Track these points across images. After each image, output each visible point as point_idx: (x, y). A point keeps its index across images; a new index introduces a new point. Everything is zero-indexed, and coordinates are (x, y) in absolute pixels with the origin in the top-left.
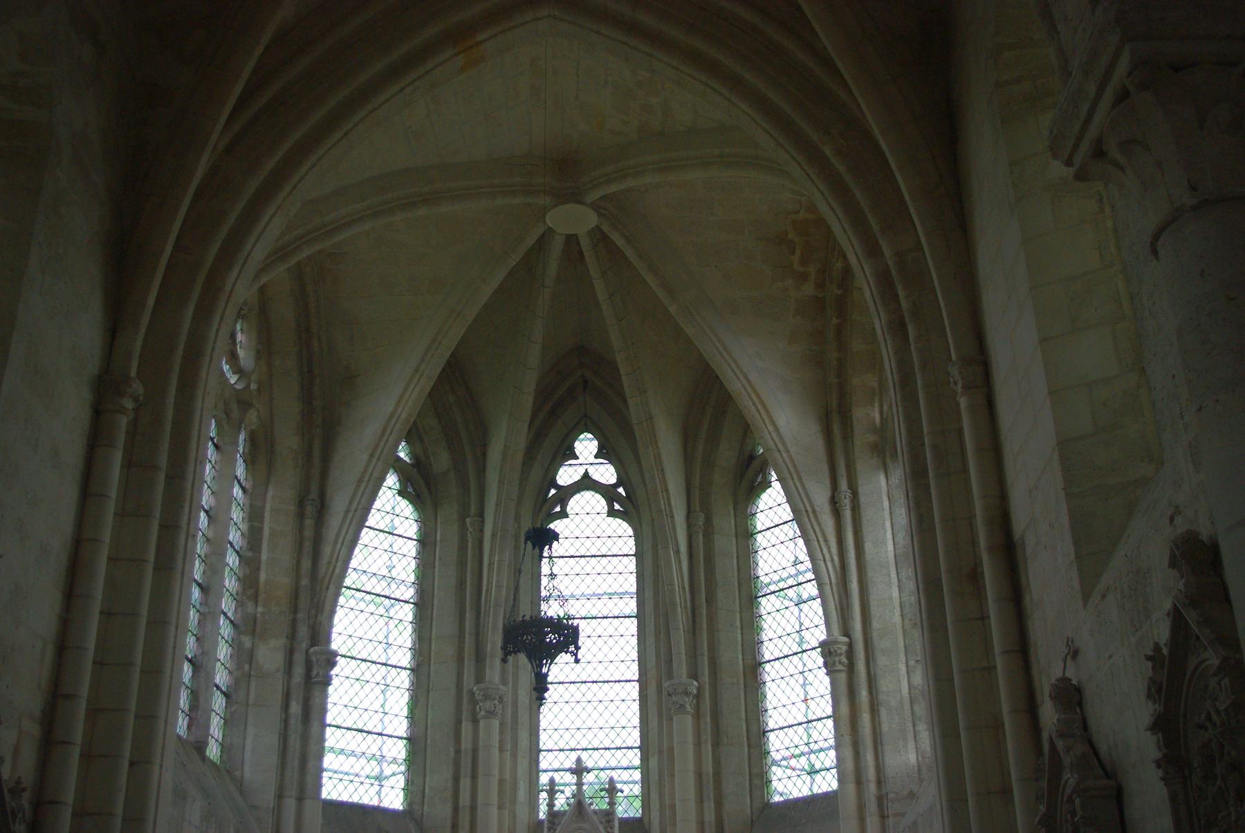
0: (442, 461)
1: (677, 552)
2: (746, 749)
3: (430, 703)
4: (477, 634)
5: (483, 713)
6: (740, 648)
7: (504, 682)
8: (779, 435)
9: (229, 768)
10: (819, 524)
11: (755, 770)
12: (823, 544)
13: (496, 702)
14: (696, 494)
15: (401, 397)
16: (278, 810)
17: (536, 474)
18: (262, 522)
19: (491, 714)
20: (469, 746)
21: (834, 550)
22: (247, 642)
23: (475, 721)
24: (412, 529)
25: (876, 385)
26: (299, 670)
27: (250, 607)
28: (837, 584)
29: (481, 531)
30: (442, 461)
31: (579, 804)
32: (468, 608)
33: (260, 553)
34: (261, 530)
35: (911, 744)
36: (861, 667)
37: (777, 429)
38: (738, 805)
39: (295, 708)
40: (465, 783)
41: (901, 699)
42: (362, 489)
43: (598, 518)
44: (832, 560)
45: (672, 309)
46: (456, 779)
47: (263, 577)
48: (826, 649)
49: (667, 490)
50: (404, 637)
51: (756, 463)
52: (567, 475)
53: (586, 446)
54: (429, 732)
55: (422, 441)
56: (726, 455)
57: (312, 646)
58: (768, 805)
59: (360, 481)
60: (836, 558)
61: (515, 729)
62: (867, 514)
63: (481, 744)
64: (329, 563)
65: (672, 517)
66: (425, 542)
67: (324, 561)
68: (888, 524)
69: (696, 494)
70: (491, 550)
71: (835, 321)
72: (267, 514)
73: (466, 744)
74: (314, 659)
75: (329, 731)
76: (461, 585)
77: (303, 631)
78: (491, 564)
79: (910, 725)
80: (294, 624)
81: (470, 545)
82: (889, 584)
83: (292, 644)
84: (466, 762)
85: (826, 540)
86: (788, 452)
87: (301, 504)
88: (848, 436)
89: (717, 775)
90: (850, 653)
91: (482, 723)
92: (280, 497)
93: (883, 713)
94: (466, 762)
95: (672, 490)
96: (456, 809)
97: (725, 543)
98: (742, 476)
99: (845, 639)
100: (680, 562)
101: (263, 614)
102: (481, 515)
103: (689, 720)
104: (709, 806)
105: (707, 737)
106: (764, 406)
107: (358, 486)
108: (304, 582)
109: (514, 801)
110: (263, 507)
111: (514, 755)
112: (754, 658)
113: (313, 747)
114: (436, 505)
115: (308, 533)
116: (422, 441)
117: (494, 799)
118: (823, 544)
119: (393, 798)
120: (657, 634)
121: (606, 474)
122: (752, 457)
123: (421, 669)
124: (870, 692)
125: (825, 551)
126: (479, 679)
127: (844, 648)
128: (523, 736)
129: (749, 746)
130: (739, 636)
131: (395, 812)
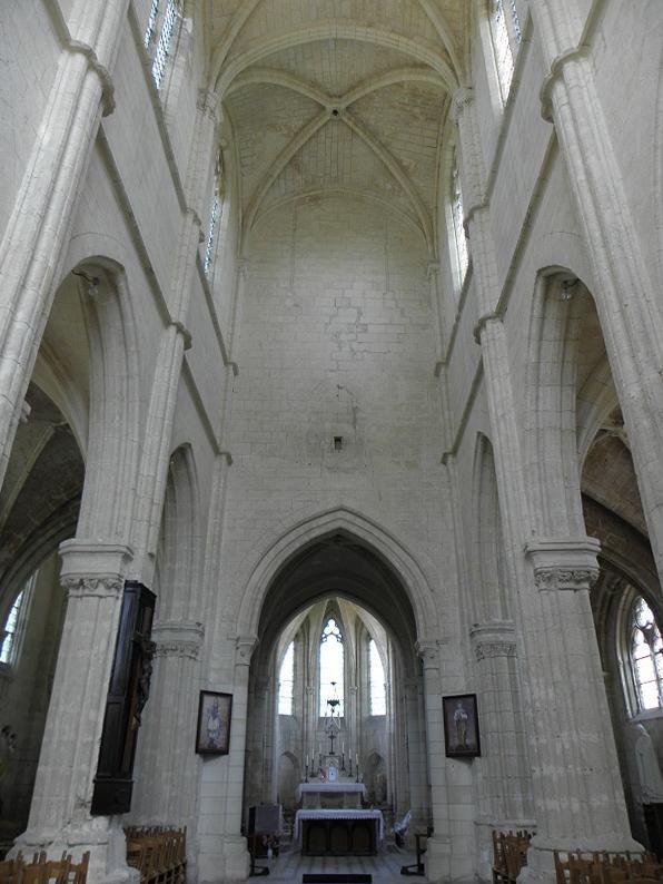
38: (365, 715)
58: (371, 716)
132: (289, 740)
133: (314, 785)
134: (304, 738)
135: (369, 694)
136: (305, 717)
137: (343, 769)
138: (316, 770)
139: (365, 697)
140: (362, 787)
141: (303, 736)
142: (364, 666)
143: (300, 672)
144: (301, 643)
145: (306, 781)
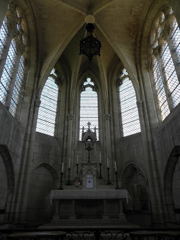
1: (106, 92)
7: (73, 114)
8: (128, 65)
9: (16, 118)
10: (136, 82)
11: (121, 131)
14: (109, 84)
15: (55, 56)
16: (27, 129)
17: (80, 82)
18: (27, 76)
19: (71, 119)
20: (67, 125)
22: (22, 96)
23: (68, 121)
24: (57, 89)
25: (146, 57)
26: (33, 103)
27: (23, 90)
29: (70, 89)
30: (63, 78)
31: (89, 130)
33: (26, 81)
34: (27, 77)
35: (157, 119)
36: (145, 105)
37: (128, 64)
39: (32, 110)
40: (66, 131)
41: (154, 110)
43: (91, 91)
44: (138, 88)
45: (108, 40)
46: (64, 131)
47: (26, 85)
50: (56, 107)
52: (85, 84)
53: (89, 80)
55: (59, 74)
56: (115, 78)
58: (123, 137)
61: (75, 123)
62: (145, 79)
63: (69, 124)
66: (59, 91)
68: (150, 81)
69: (109, 84)
71: (139, 45)
72: (28, 75)
73: (66, 124)
74: (36, 101)
76: (66, 98)
77: (34, 96)
78: (72, 94)
79: (156, 115)
80: (32, 96)
82: (151, 91)
84: (66, 128)
85: (137, 84)
87: (35, 75)
89: (114, 131)
90: (143, 103)
92: (32, 71)
93: (151, 113)
94: (66, 128)
96: (64, 136)
97: (114, 93)
98: (117, 82)
101: (26, 92)
103: (109, 121)
104: (113, 136)
105: (112, 124)
106: (125, 60)
107: (47, 71)
109: (75, 136)
110: (27, 74)
111: (75, 128)
113: (35, 118)
114: (62, 86)
116: (59, 74)
117: (71, 134)
119: (52, 134)
120: (102, 108)
121: (92, 84)
122: (119, 79)
123: (59, 102)
124: (147, 110)
126: (69, 113)
127: (142, 103)
128: (77, 125)
134: (64, 154)
136: (65, 138)
137: (100, 178)
140: (124, 194)
141: (62, 153)
142: (115, 101)
143: (63, 104)
144: (64, 86)
145: (61, 188)
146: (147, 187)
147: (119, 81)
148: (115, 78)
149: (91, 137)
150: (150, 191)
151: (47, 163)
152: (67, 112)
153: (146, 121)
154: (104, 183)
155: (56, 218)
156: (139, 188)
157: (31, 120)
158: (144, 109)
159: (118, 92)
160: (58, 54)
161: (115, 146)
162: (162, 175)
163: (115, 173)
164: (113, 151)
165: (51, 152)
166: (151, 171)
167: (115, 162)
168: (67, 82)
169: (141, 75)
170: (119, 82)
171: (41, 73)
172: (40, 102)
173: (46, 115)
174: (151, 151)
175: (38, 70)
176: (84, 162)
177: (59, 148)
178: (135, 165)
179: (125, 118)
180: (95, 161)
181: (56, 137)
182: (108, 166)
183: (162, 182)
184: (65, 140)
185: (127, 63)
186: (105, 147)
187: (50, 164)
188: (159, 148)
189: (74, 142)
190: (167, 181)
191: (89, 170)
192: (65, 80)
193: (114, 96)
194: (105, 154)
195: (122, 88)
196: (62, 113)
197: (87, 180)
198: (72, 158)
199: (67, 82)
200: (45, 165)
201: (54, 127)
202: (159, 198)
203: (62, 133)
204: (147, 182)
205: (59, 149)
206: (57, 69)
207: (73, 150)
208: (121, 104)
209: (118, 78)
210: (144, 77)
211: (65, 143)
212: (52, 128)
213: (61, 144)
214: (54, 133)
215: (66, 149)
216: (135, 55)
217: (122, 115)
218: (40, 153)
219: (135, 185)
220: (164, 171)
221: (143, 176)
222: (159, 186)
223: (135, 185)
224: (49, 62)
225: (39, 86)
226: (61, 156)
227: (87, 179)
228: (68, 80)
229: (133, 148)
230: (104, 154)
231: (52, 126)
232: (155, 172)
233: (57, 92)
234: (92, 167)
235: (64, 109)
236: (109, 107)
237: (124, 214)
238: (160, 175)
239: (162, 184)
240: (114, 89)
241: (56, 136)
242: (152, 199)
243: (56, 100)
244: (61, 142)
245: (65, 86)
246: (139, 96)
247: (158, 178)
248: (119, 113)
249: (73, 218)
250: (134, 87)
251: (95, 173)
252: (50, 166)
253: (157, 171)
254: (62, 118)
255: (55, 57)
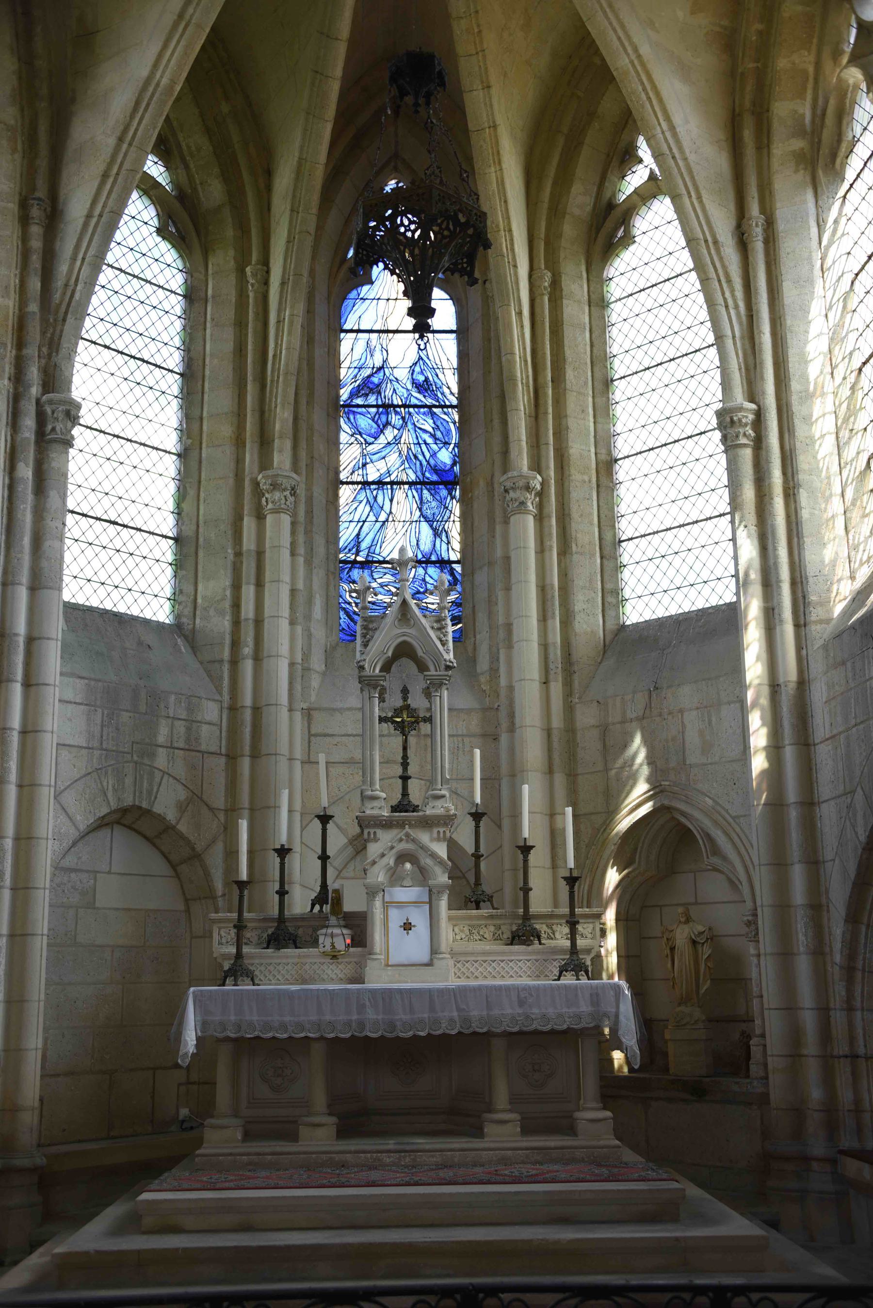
0: (213, 192)
1: (520, 314)
2: (599, 561)
3: (202, 495)
4: (262, 412)
5: (270, 506)
6: (592, 440)
8: (675, 135)
10: (721, 259)
11: (609, 586)
12: (725, 285)
13: (287, 493)
15: (160, 56)
21: (739, 294)
23: (260, 517)
24: (177, 281)
26: (29, 423)
28: (742, 338)
30: (213, 192)
32: (250, 378)
38: (589, 623)
40: (248, 592)
42: (108, 186)
44: (736, 307)
46: (236, 587)
48: (726, 421)
49: (510, 230)
50: (171, 414)
51: (616, 214)
54: (201, 530)
55: (187, 167)
56: (580, 200)
57: (43, 394)
58: (623, 627)
59: (105, 176)
60: (742, 305)
64: (66, 285)
65: (515, 266)
67: (59, 283)
70: (280, 303)
73: (249, 543)
74: (49, 410)
75: (82, 344)
76: (240, 350)
77: (34, 373)
81: (251, 301)
83: (16, 389)
85: (729, 281)
86: (685, 159)
87: (24, 205)
88: (764, 143)
91: (269, 519)
95: (516, 233)
96: (236, 623)
97: (575, 311)
98: (598, 230)
99: (753, 406)
100: (522, 326)
102: (265, 262)
103: (530, 521)
105: (553, 543)
108: (33, 307)
112: (610, 453)
114: (206, 253)
115: (36, 244)
116: (187, 167)
117: (285, 611)
118: (725, 285)
122: (611, 206)
123: (191, 376)
124: (784, 473)
125: (728, 294)
126: (265, 463)
127: (751, 417)
129: (602, 558)
130: (592, 425)
131: (160, 625)
132: (148, 749)
133: (296, 985)
135: (608, 518)
138: (300, 902)
139: (585, 531)
142: (577, 377)
143: (218, 399)
144: (223, 260)
146: (752, 951)
147: (609, 224)
148: (580, 200)
149: (420, 653)
150: (763, 974)
151: (144, 805)
152: (250, 457)
153: (770, 547)
154: (498, 927)
155: (222, 1138)
156: (706, 951)
157: (27, 541)
158: (763, 462)
159: (599, 303)
160: (180, 48)
161: (568, 683)
162: (838, 894)
163: (565, 878)
164: (557, 722)
165: (162, 735)
166: (779, 864)
167: (569, 810)
168: (243, 228)
169: (763, 211)
170: (609, 230)
171: (62, 192)
172: (71, 413)
173: (114, 479)
174: (787, 742)
175: (43, 163)
176: (375, 812)
177: (211, 704)
178: (683, 814)
179: (639, 496)
180: (439, 803)
181: (182, 630)
182: (526, 833)
183: (837, 929)
184: (247, 650)
185: (668, 119)
186: (503, 693)
187: (158, 809)
188: (835, 732)
189: (306, 656)
190: (863, 928)
191: (402, 858)
192: (227, 212)
193: (568, 333)
194: (504, 738)
195: (625, 271)
196: (218, 456)
197: (396, 918)
198: (298, 765)
199: (243, 228)
200: (128, 819)
201: (170, 557)
202: (809, 1020)
203: (223, 599)
204: (748, 924)
205: (211, 711)
206: (190, 178)
207: (298, 716)
208: (620, 391)
209: (607, 194)
210: (781, 226)
211: (248, 666)
212: (157, 569)
213: (221, 678)
214: (174, 599)
215: (257, 710)
216: (729, 43)
217: (614, 318)
218: (96, 744)
219: (682, 935)
220: (853, 876)
221: (734, 885)
222: (819, 951)
223: (682, 935)
224: (120, 102)
225: (57, 296)
226: (227, 756)
227: (393, 913)
228: (253, 216)
229: (681, 711)
230: (496, 739)
231: (158, 554)
232: (798, 875)
233: (176, 304)
234: (424, 837)
235: (227, 430)
236: (537, 417)
237: (605, 1108)
238: (827, 892)
239: (837, 946)
240: (576, 288)
241: (184, 620)
242: (772, 1026)
243: (175, 360)
244: (221, 661)
245: (231, 253)
246: (734, 364)
247: (817, 907)
248: (603, 457)
249: (319, 1137)
250: (704, 281)
251: (442, 878)
252: (161, 818)
253: (814, 863)
254: (217, 502)
255: (156, 66)
